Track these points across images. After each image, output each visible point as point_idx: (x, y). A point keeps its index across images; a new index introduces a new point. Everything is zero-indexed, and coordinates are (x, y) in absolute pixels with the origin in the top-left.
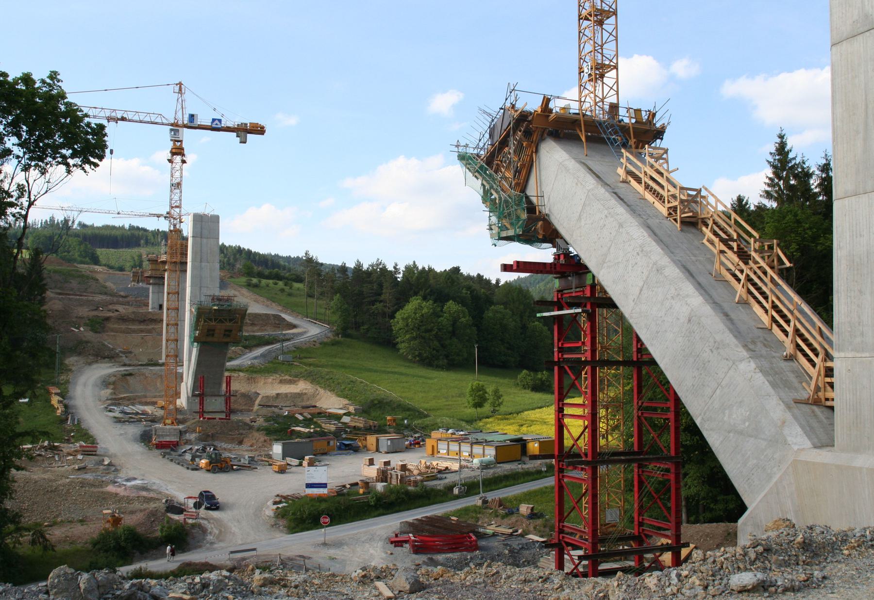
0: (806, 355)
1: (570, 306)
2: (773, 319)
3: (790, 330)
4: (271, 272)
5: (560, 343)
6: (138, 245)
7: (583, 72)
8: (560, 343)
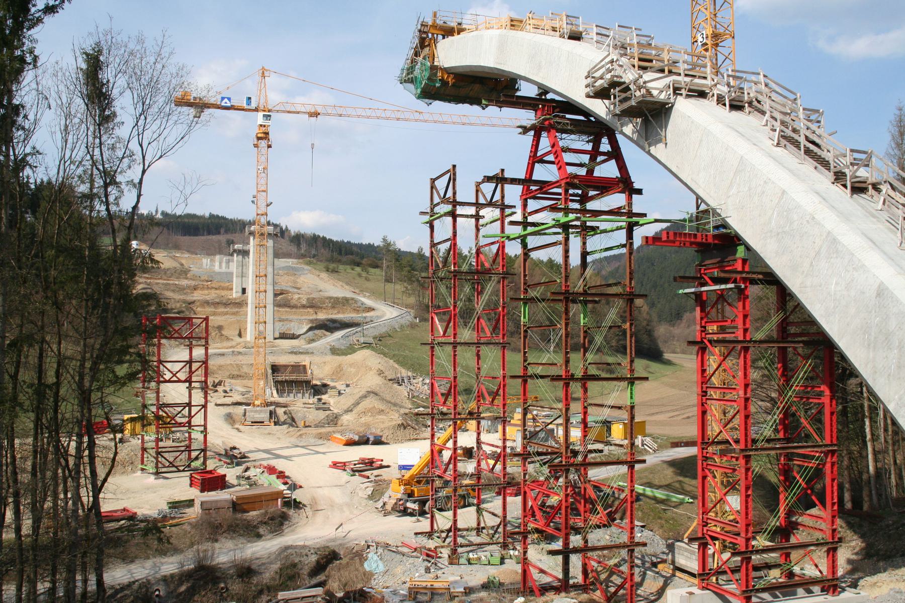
5: (703, 322)
7: (696, 41)
8: (703, 322)
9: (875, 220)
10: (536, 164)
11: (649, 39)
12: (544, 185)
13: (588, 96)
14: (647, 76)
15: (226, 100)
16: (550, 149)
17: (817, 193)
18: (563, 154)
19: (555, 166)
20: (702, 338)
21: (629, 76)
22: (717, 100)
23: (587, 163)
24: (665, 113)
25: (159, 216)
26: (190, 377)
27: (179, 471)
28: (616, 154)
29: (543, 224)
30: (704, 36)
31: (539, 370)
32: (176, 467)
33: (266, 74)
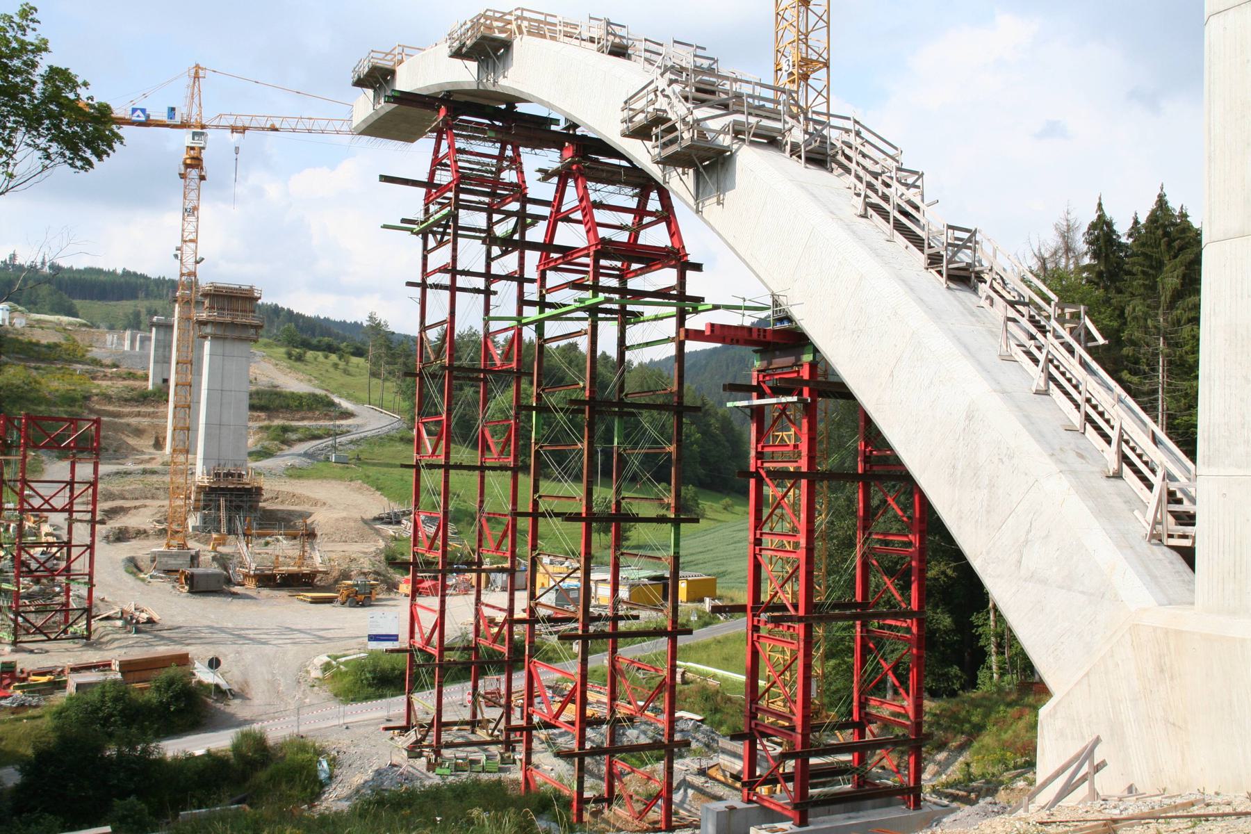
0: (1137, 472)
1: (776, 392)
2: (1088, 418)
3: (1114, 435)
4: (319, 342)
5: (760, 446)
6: (133, 296)
7: (780, 70)
8: (760, 446)
9: (973, 319)
10: (560, 223)
11: (712, 62)
12: (567, 251)
13: (624, 135)
14: (701, 113)
15: (139, 112)
16: (577, 203)
17: (903, 281)
18: (595, 211)
19: (582, 226)
20: (757, 468)
21: (677, 110)
22: (791, 151)
23: (630, 224)
24: (723, 164)
25: (46, 270)
26: (71, 503)
27: (50, 639)
28: (667, 215)
29: (565, 305)
30: (791, 64)
31: (557, 506)
32: (45, 634)
33: (201, 73)
